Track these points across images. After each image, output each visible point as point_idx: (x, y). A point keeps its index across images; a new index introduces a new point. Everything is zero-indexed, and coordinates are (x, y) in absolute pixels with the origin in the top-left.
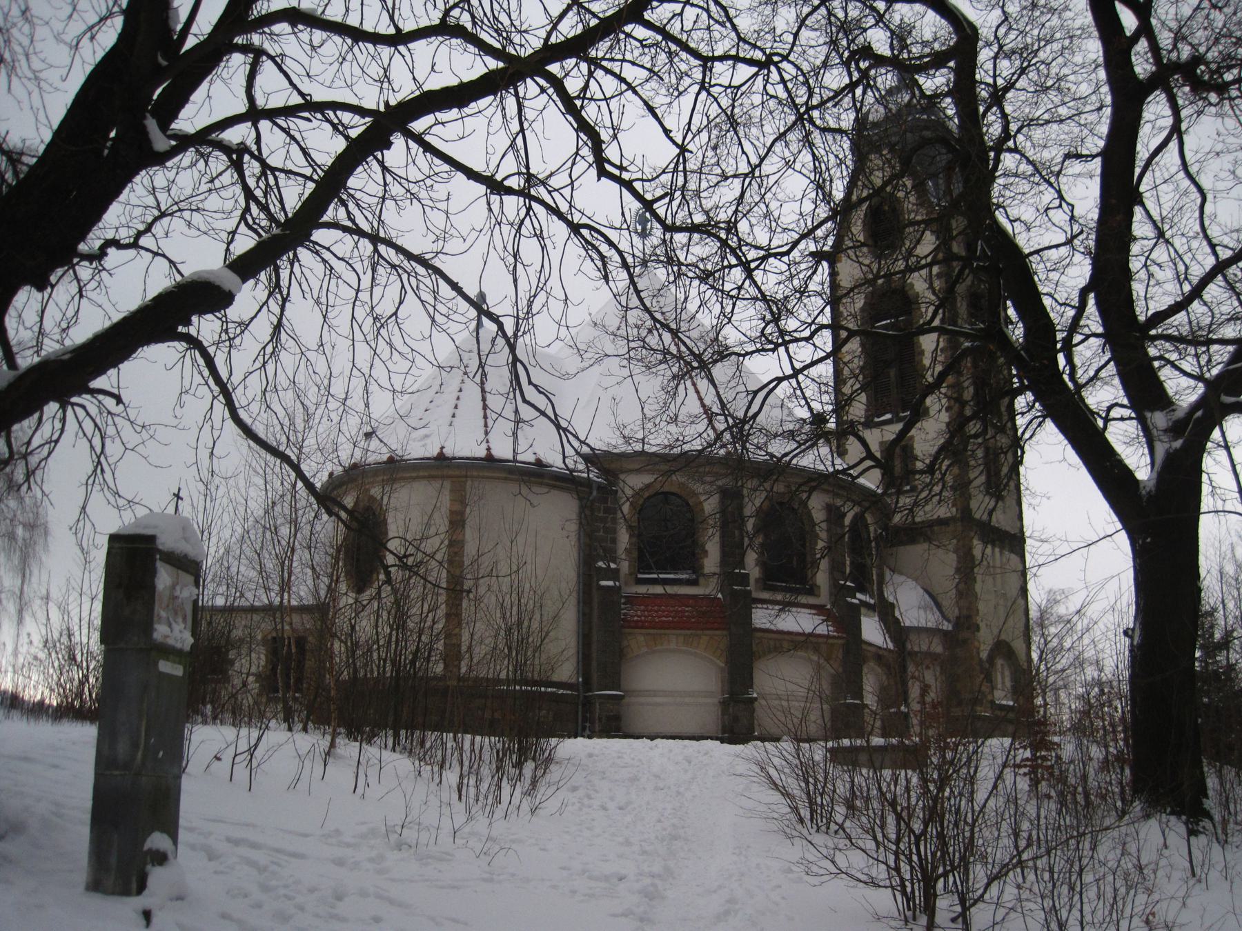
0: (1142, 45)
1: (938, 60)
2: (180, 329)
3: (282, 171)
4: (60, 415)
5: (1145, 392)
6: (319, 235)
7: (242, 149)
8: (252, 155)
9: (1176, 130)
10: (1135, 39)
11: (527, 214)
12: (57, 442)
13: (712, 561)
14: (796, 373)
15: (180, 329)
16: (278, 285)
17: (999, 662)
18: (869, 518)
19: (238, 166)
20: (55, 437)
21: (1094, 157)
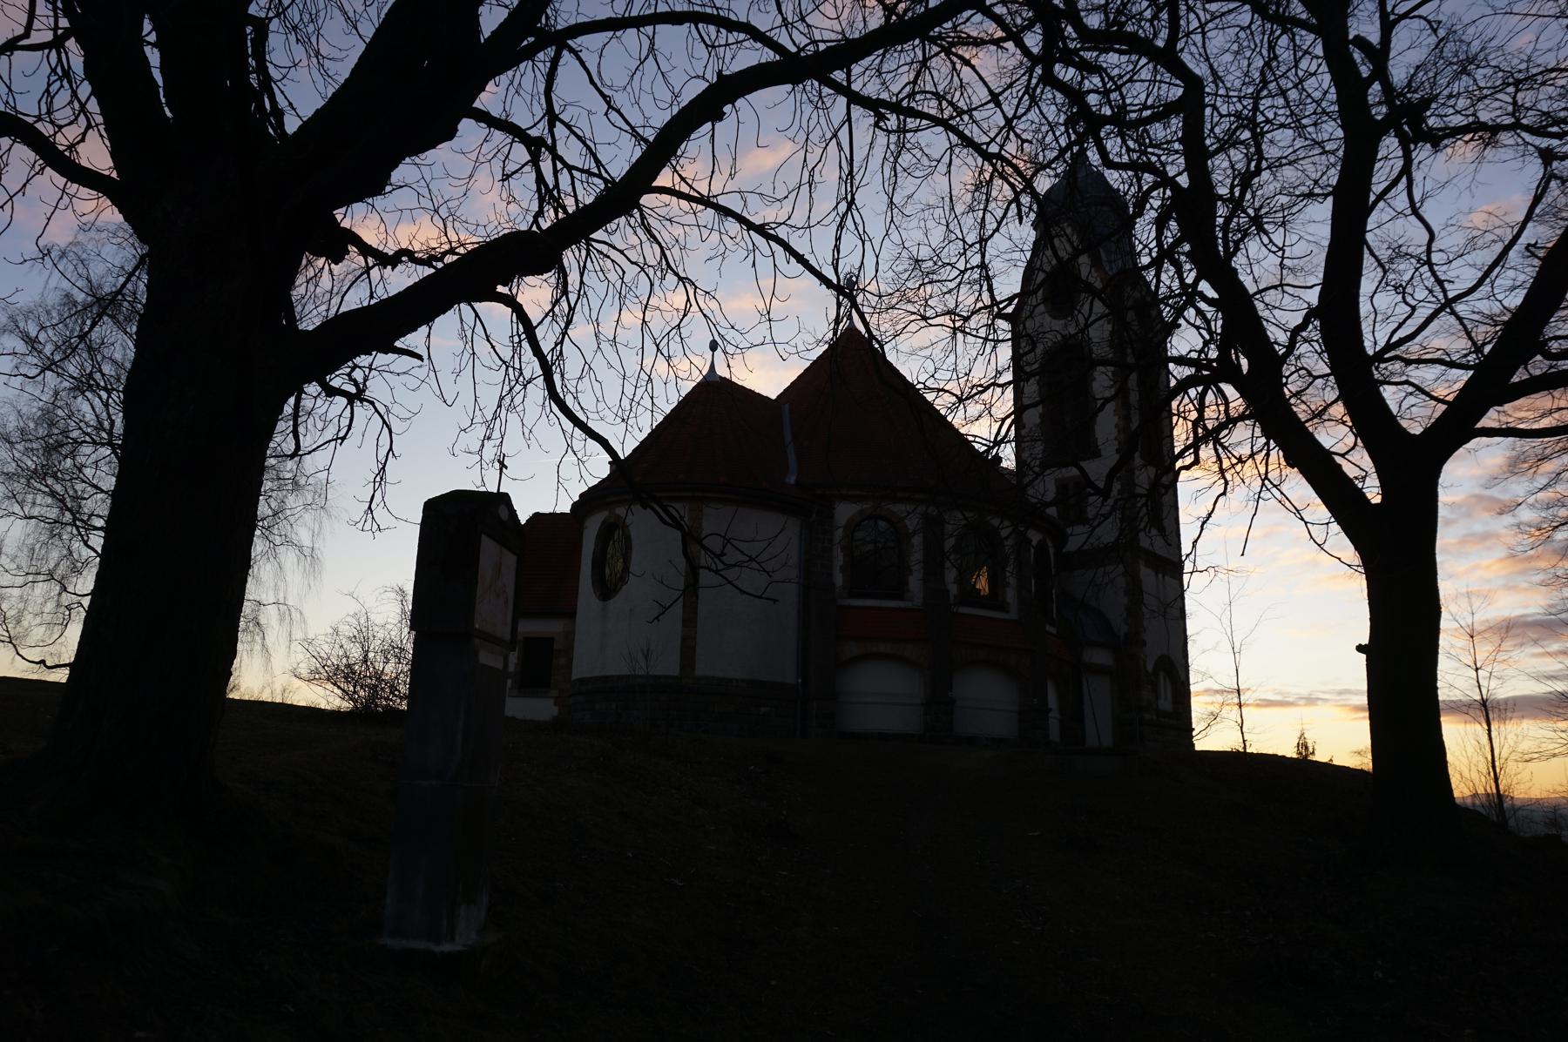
0: (1376, 86)
1: (1164, 112)
2: (500, 289)
3: (582, 171)
4: (347, 413)
5: (1373, 423)
6: (647, 200)
7: (540, 141)
8: (548, 148)
9: (1406, 170)
10: (1369, 82)
11: (849, 208)
12: (343, 439)
13: (915, 583)
14: (1448, 304)
15: (500, 289)
16: (565, 292)
17: (1162, 674)
18: (1049, 543)
19: (535, 161)
20: (341, 434)
21: (1326, 196)
